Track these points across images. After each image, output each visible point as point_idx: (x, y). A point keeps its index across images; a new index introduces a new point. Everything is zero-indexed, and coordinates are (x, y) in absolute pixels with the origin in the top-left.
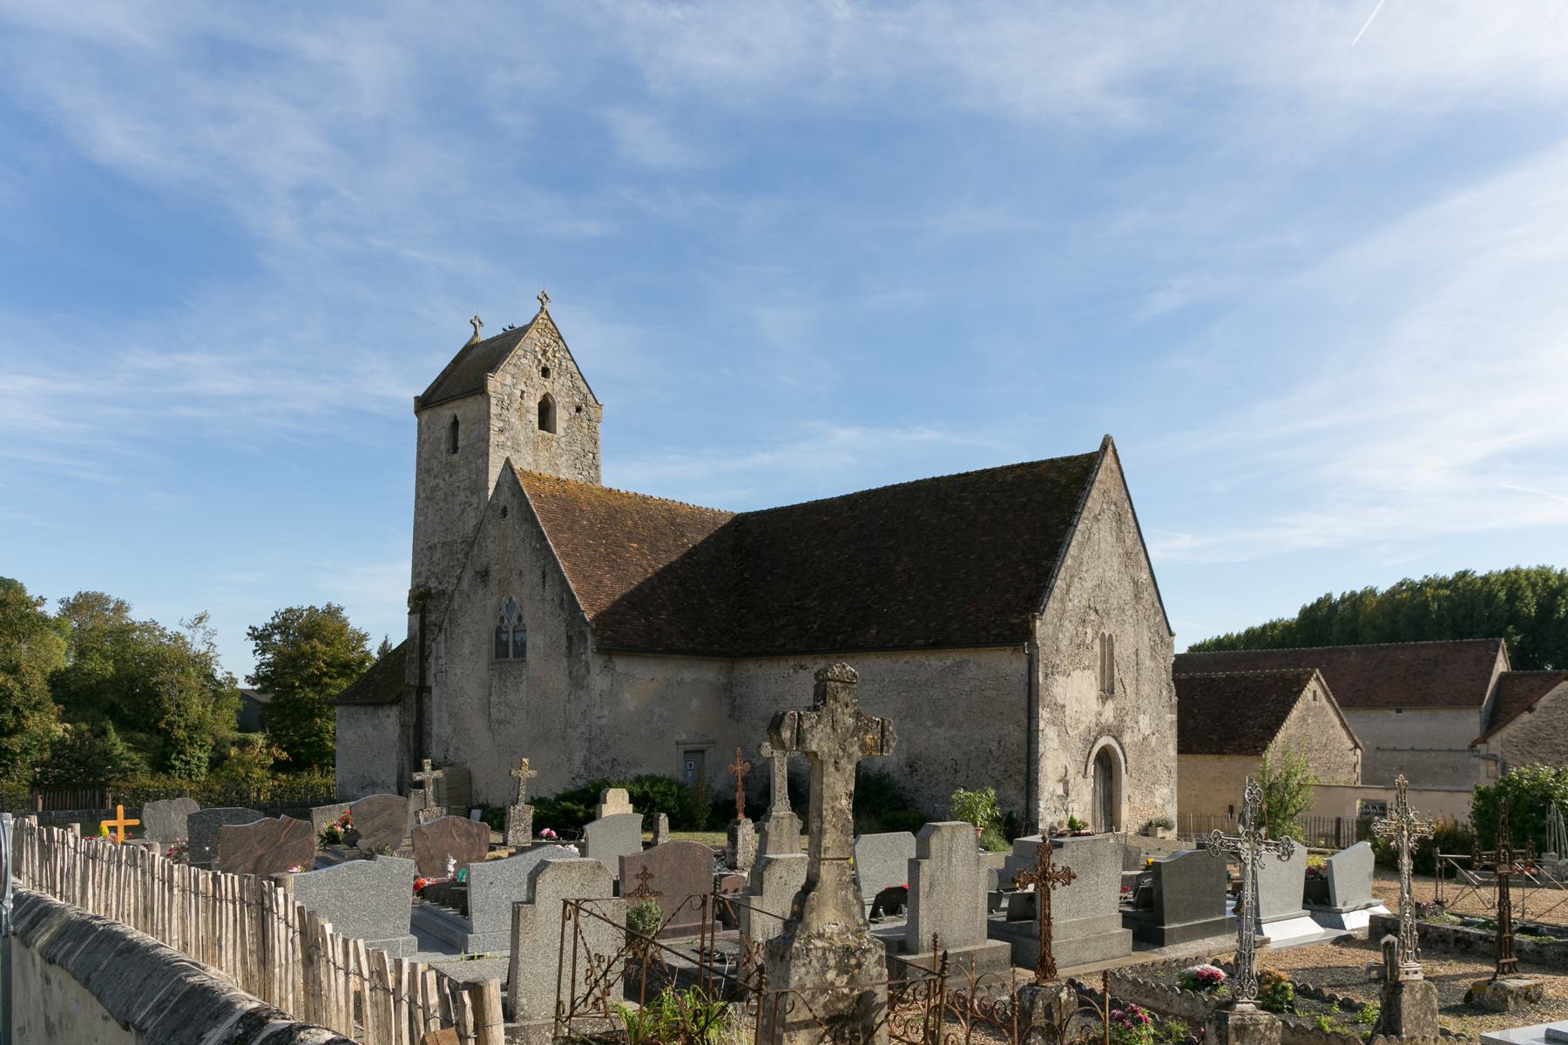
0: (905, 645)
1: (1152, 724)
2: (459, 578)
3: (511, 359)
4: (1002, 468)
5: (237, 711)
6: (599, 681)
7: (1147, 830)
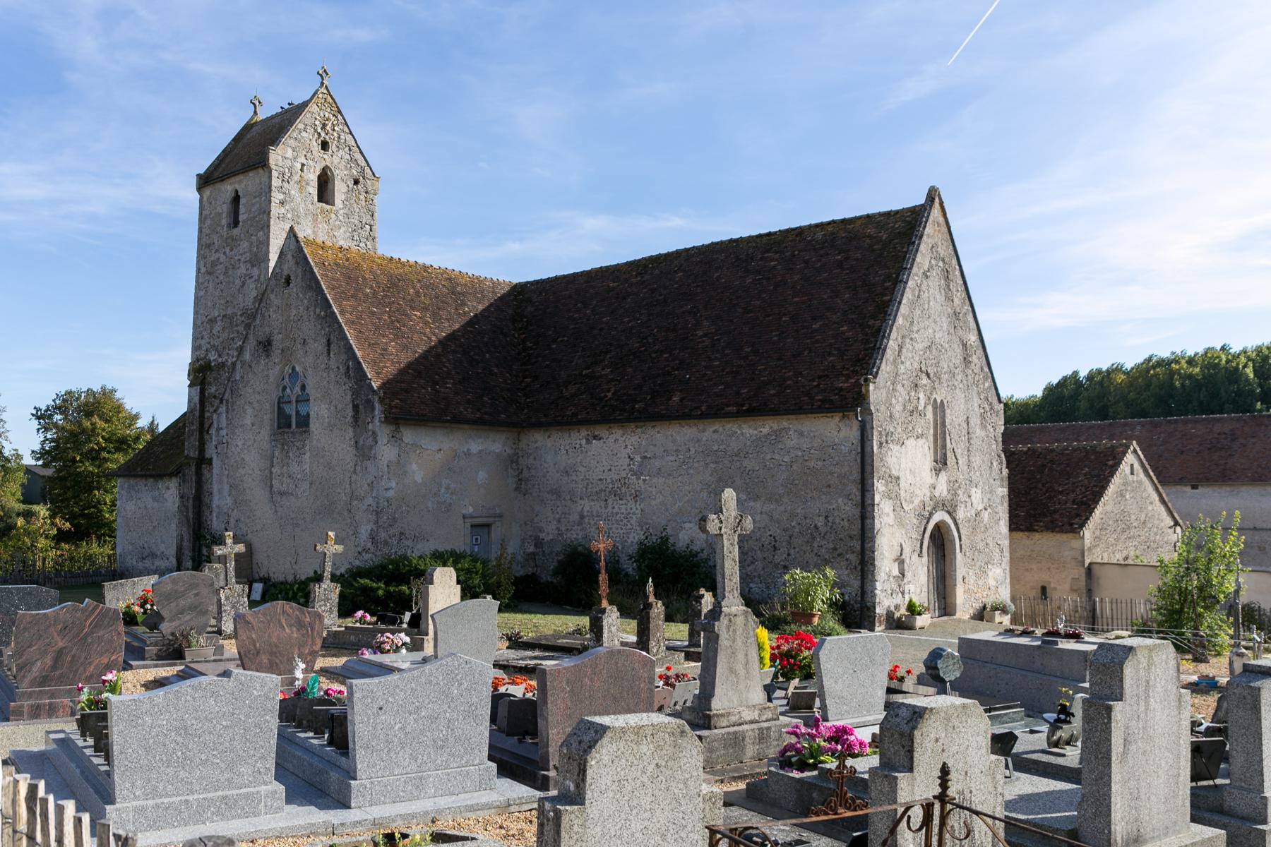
0: (716, 413)
1: (984, 498)
2: (241, 350)
3: (292, 132)
4: (810, 226)
5: (22, 485)
6: (386, 452)
7: (981, 615)
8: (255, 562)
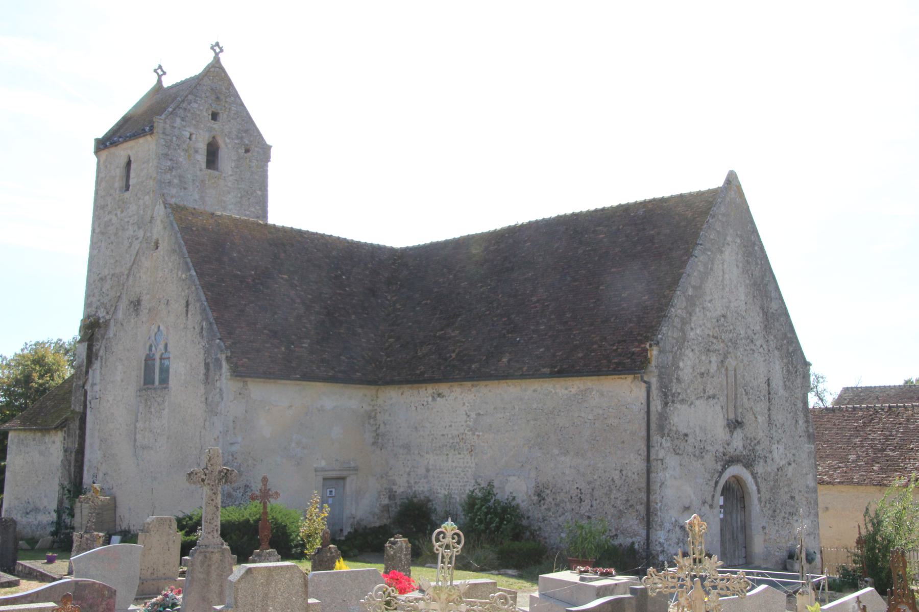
8: (117, 515)
